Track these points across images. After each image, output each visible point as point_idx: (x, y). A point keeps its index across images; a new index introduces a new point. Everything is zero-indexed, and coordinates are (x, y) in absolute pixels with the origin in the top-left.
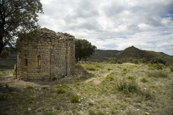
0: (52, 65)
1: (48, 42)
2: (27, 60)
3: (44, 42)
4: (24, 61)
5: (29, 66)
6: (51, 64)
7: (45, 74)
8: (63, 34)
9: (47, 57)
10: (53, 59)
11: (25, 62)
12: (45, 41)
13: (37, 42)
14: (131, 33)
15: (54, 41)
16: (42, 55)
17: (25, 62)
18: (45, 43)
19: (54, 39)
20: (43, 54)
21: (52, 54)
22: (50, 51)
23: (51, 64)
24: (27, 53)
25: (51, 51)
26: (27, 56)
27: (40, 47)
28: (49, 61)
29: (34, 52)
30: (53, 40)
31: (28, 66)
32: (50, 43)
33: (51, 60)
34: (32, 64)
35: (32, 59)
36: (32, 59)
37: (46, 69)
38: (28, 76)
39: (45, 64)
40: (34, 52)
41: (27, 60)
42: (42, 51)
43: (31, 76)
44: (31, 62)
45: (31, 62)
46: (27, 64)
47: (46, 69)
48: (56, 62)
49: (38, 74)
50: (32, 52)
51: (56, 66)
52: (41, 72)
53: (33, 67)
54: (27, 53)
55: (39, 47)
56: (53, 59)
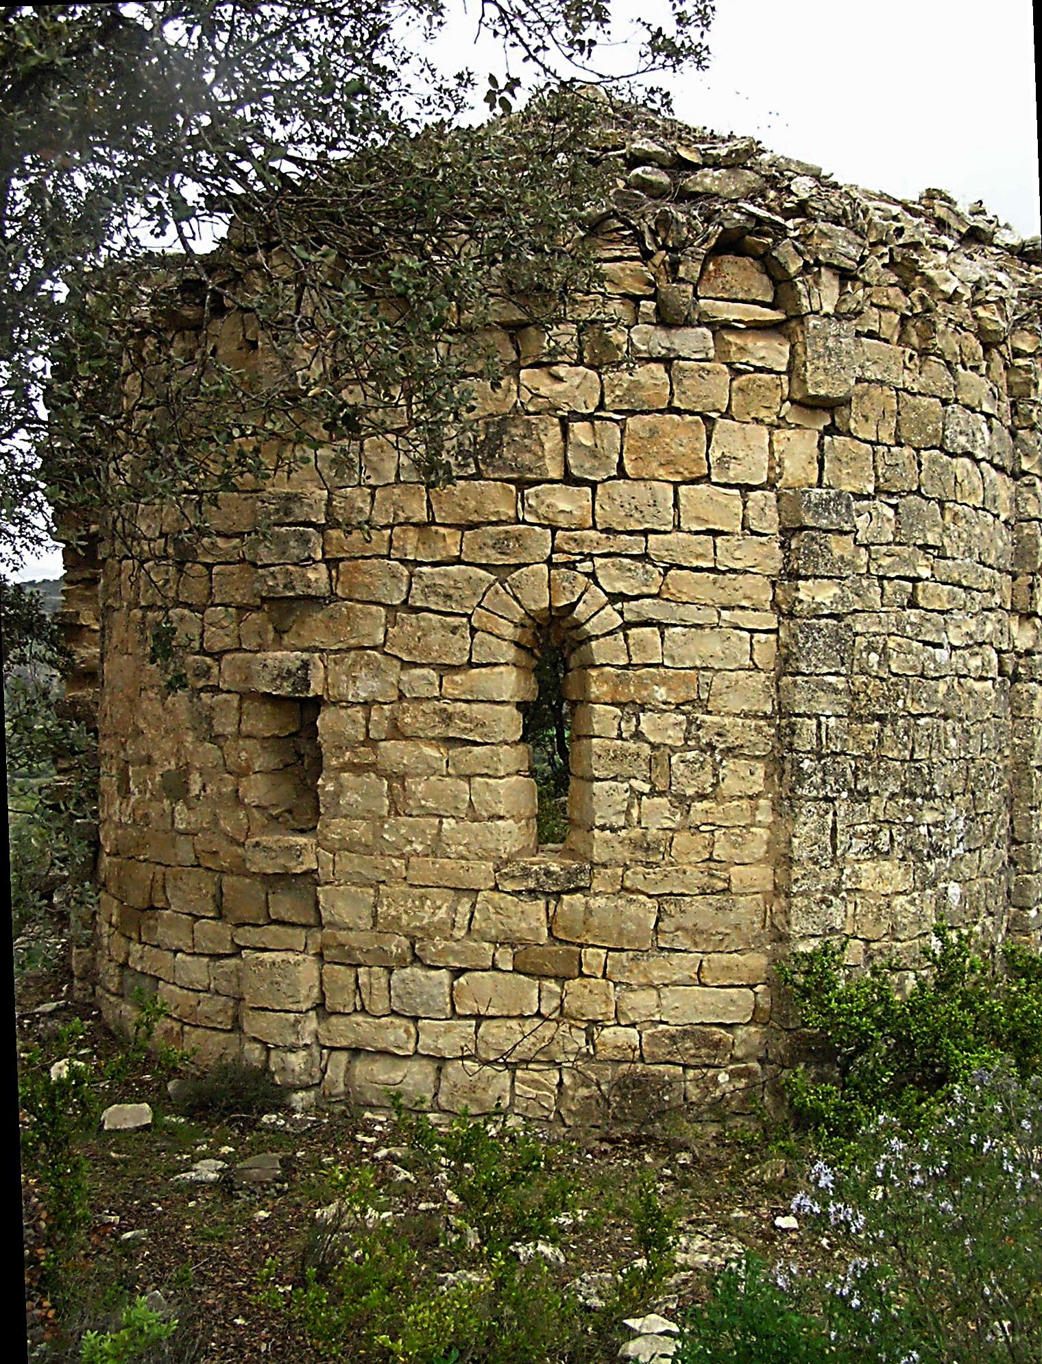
0: (806, 827)
1: (720, 327)
2: (317, 703)
3: (660, 340)
4: (261, 722)
5: (360, 830)
6: (787, 805)
7: (670, 997)
8: (771, 277)
9: (710, 646)
10: (824, 705)
11: (273, 761)
12: (667, 319)
13: (515, 330)
14: (747, 261)
15: (839, 316)
16: (614, 598)
17: (273, 761)
18: (667, 361)
19: (845, 276)
20: (621, 587)
21: (806, 591)
22: (770, 523)
23: (787, 805)
24: (318, 576)
25: (788, 532)
26: (315, 629)
27: (579, 430)
28: (739, 732)
29: (452, 544)
30: (827, 295)
31: (335, 829)
32: (774, 353)
33: (783, 711)
34: (418, 787)
35: (422, 680)
36: (422, 680)
37: (699, 910)
38: (343, 1031)
39: (683, 802)
40: (452, 544)
41: (317, 703)
42: (449, 689)
43: (396, 1034)
44: (394, 752)
45: (394, 752)
46: (312, 792)
47: (699, 910)
48: (873, 759)
49: (530, 994)
50: (411, 544)
51: (876, 853)
52: (593, 958)
53: (436, 848)
54: (318, 576)
55: (552, 438)
56: (824, 705)
